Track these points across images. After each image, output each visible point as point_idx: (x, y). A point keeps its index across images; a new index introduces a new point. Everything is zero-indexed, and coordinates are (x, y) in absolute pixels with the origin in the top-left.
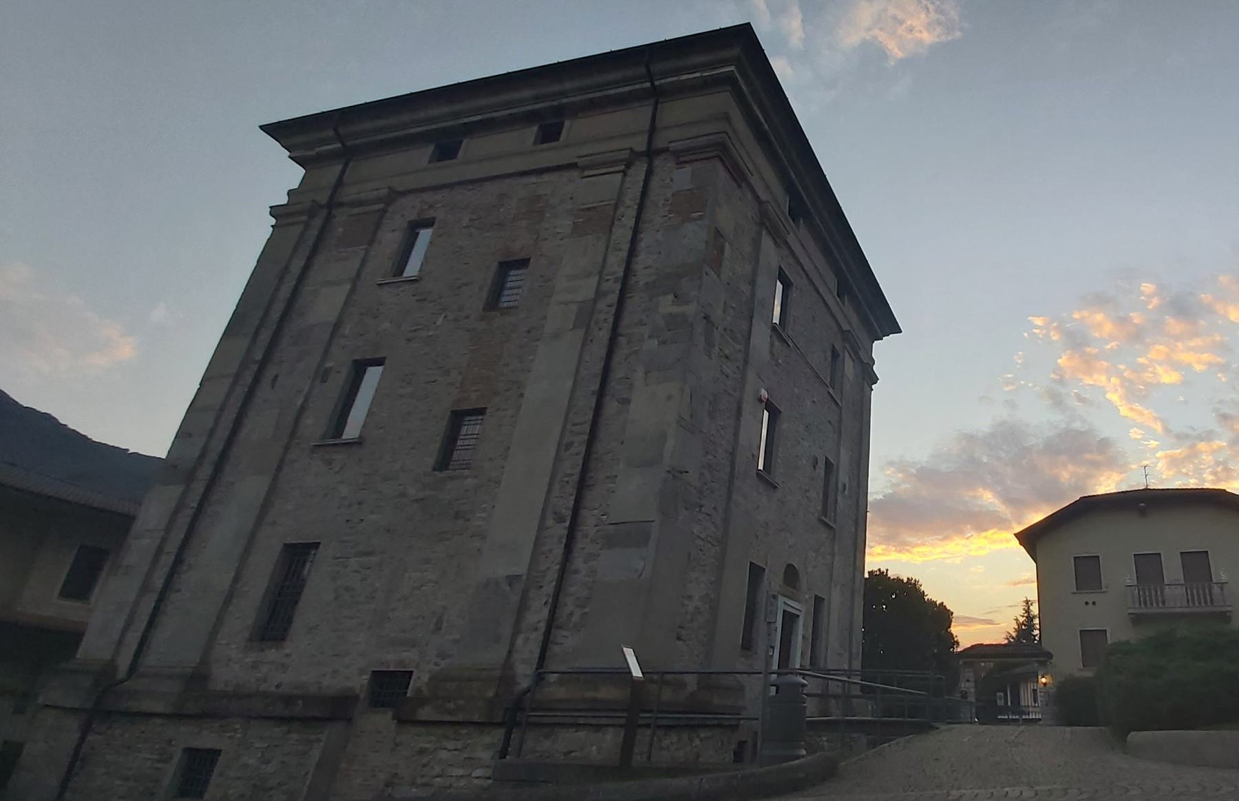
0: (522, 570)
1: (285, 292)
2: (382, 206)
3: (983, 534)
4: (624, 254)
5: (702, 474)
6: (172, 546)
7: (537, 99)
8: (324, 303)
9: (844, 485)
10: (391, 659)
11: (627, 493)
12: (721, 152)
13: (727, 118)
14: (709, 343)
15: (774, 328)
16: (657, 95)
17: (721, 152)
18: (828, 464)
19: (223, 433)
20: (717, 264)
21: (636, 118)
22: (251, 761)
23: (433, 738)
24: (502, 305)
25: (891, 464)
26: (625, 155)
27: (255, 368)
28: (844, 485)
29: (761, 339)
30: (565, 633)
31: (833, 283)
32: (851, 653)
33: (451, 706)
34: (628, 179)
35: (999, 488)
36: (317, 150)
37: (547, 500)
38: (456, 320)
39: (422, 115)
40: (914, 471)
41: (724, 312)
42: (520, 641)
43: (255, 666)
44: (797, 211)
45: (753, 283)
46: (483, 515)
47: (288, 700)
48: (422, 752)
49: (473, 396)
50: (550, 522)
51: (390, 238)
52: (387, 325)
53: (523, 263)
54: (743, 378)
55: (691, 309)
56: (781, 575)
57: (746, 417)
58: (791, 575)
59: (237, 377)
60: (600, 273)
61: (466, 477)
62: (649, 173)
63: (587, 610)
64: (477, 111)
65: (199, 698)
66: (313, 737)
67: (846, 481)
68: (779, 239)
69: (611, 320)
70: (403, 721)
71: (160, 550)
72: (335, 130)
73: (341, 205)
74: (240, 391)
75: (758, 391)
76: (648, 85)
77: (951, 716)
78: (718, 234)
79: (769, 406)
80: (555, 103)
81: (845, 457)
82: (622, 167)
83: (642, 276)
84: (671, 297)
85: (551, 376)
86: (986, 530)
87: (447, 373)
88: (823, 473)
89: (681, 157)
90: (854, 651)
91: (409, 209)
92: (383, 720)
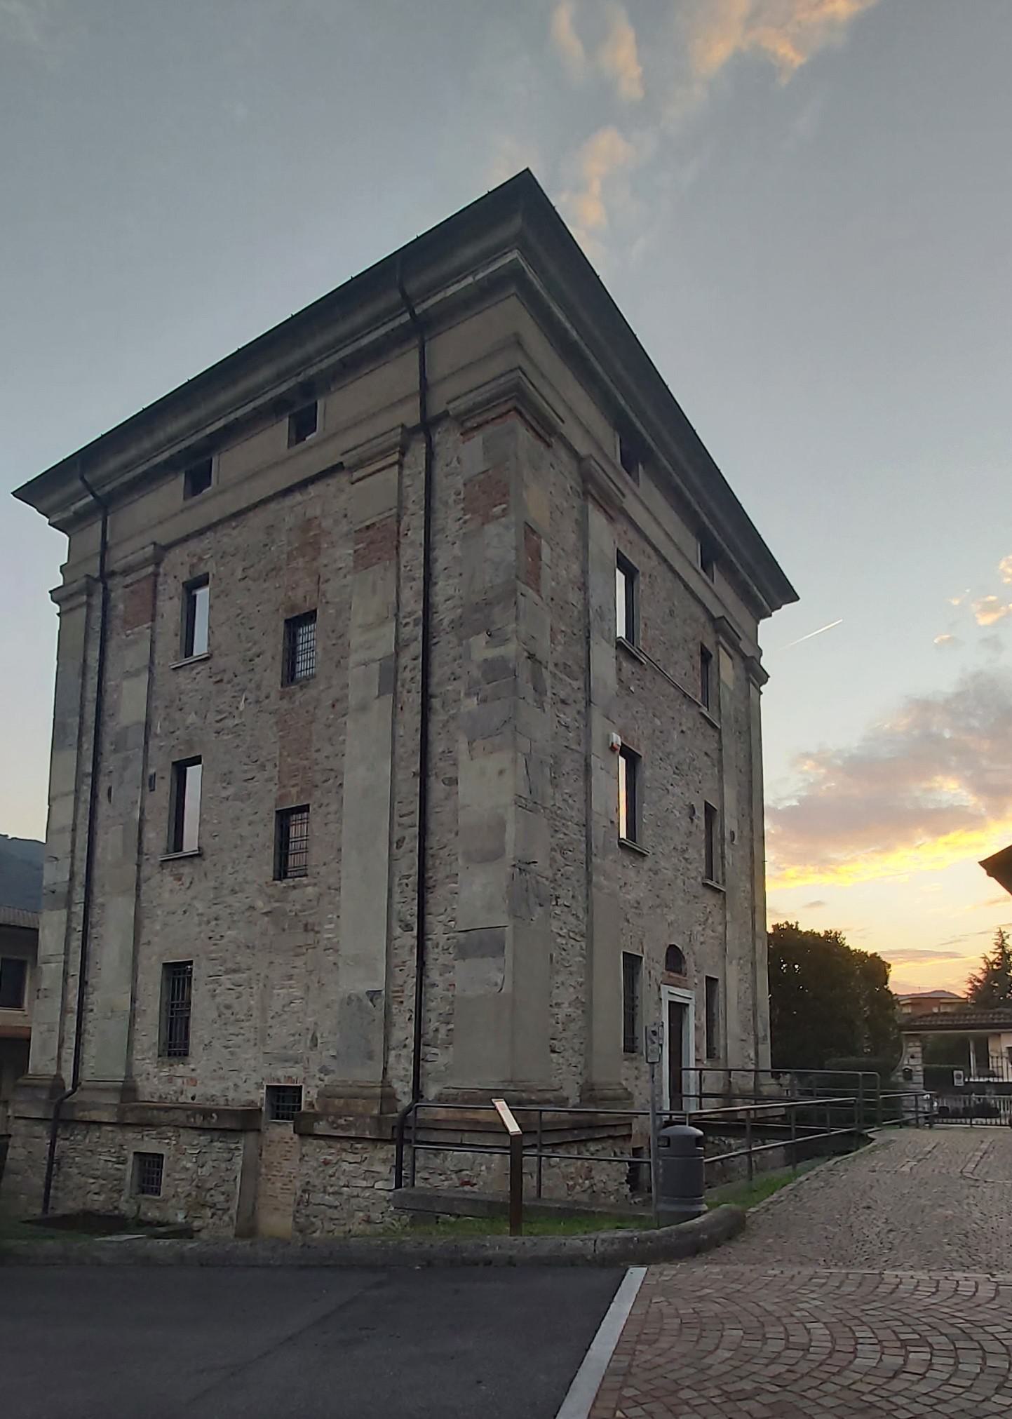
0: (379, 985)
1: (91, 694)
2: (150, 569)
3: (942, 839)
4: (419, 584)
5: (553, 860)
6: (75, 970)
7: (280, 377)
8: (129, 703)
9: (732, 834)
10: (283, 1075)
11: (472, 895)
12: (518, 401)
13: (518, 342)
14: (539, 690)
15: (619, 645)
16: (421, 329)
17: (518, 401)
18: (709, 810)
19: (82, 854)
20: (534, 578)
21: (398, 374)
22: (189, 1165)
23: (333, 1151)
24: (298, 675)
25: (807, 756)
26: (396, 437)
27: (89, 781)
28: (732, 834)
29: (604, 661)
30: (435, 1050)
31: (693, 549)
32: (756, 1035)
33: (342, 1121)
34: (406, 472)
35: (968, 773)
36: (73, 508)
37: (389, 906)
38: (257, 702)
39: (160, 436)
40: (839, 762)
41: (552, 642)
42: (392, 1059)
43: (170, 1079)
44: (634, 455)
45: (584, 587)
46: (332, 926)
47: (206, 1113)
48: (326, 1163)
49: (294, 790)
50: (398, 931)
51: (170, 608)
52: (192, 718)
53: (310, 617)
54: (588, 725)
55: (511, 649)
56: (663, 959)
57: (598, 776)
58: (674, 959)
59: (77, 790)
60: (396, 615)
61: (306, 886)
62: (430, 456)
63: (451, 1026)
64: (218, 414)
65: (134, 1111)
66: (233, 1146)
67: (735, 829)
68: (613, 510)
69: (419, 677)
70: (305, 1134)
71: (66, 974)
72: (82, 478)
73: (113, 574)
74: (84, 809)
75: (608, 737)
76: (407, 317)
77: (892, 1115)
78: (530, 531)
79: (625, 751)
80: (300, 379)
81: (730, 795)
82: (396, 457)
83: (445, 614)
84: (483, 637)
85: (365, 764)
86: (946, 833)
87: (263, 767)
88: (703, 826)
89: (467, 421)
90: (761, 1034)
91: (178, 566)
92: (286, 1130)
